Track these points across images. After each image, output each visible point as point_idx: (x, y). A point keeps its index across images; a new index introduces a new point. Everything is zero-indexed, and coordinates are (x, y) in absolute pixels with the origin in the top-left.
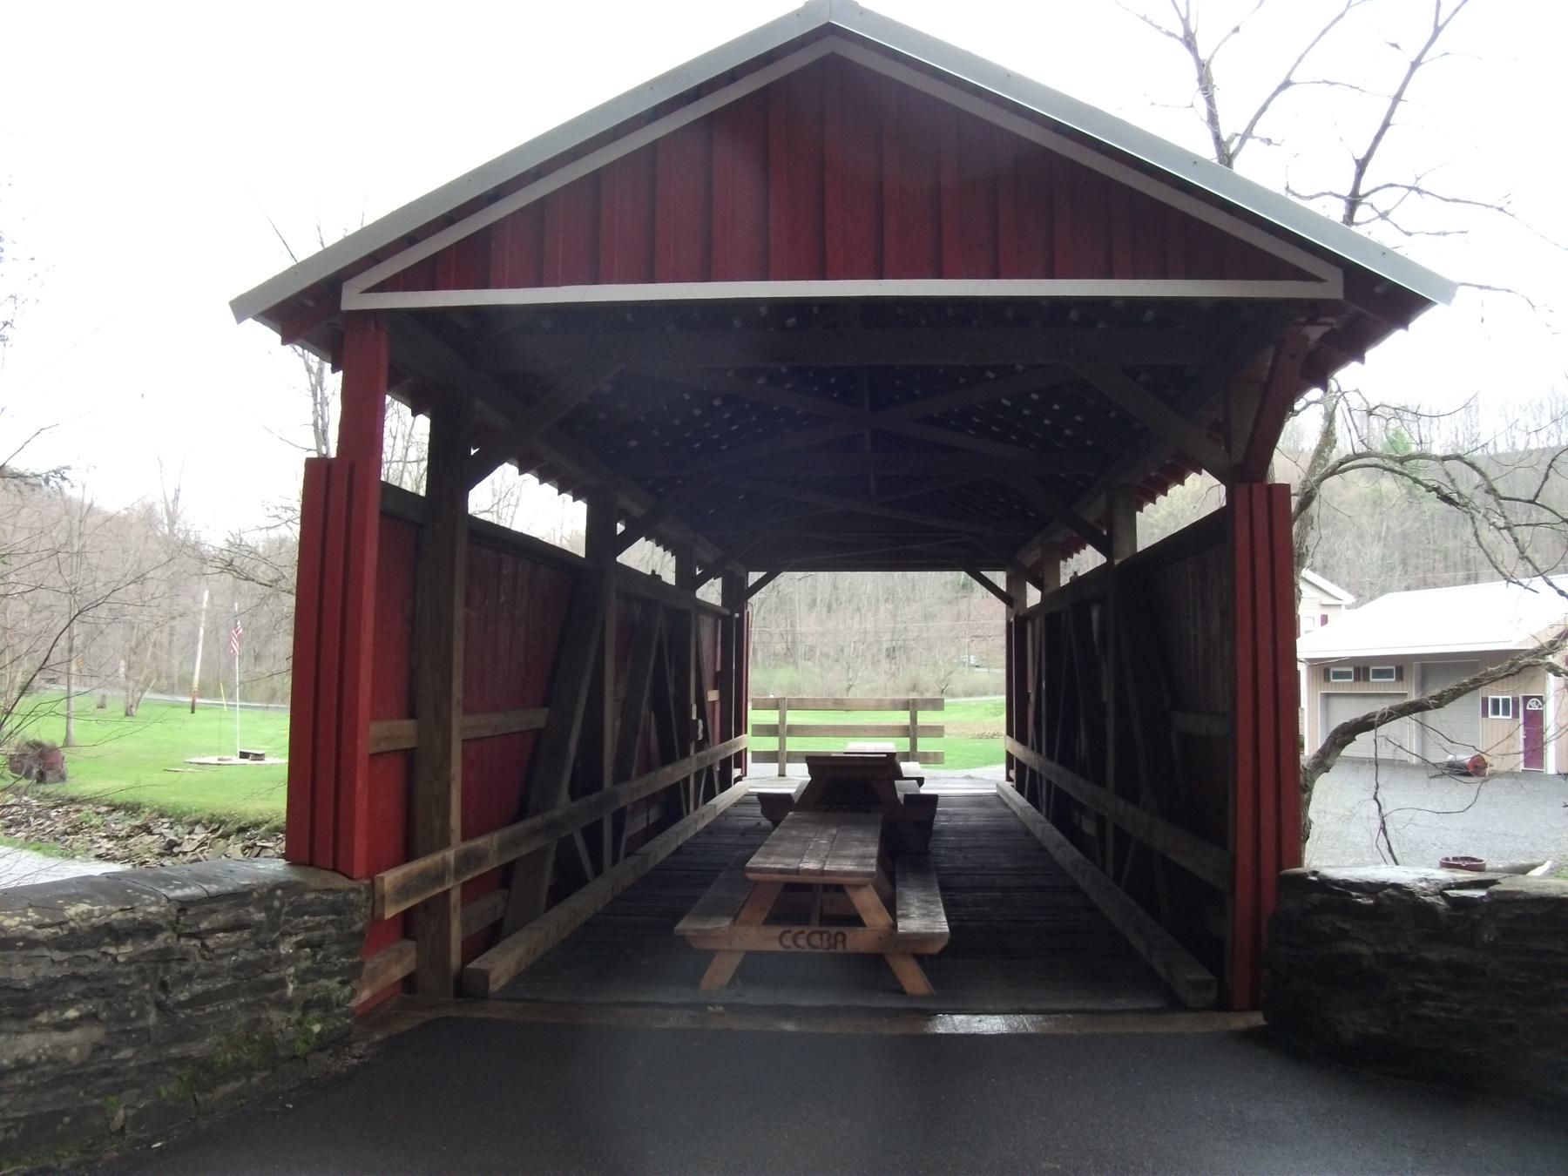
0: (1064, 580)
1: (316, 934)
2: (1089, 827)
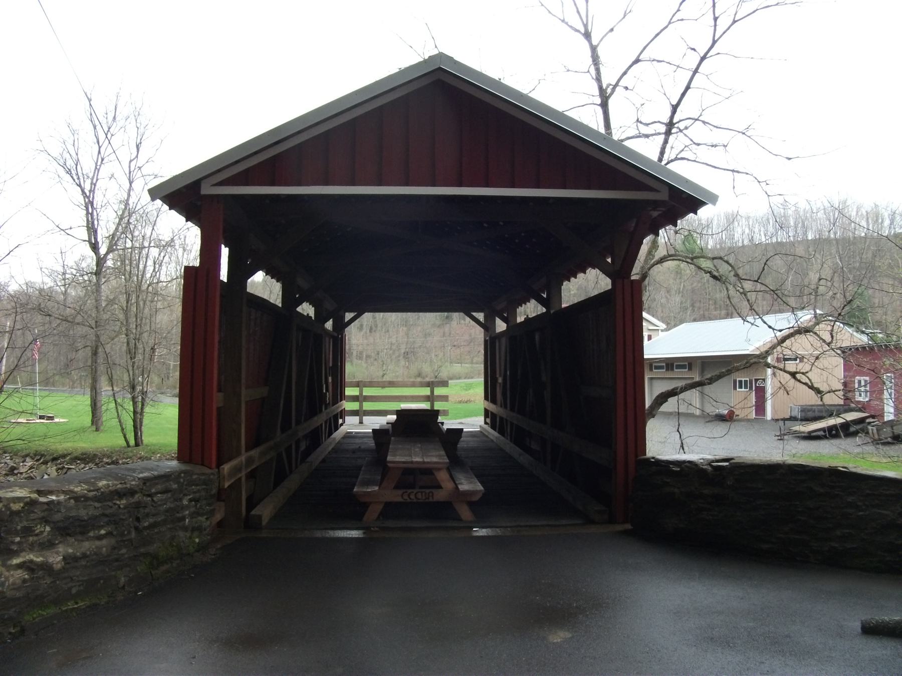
0: (520, 319)
1: (197, 495)
2: (535, 446)
